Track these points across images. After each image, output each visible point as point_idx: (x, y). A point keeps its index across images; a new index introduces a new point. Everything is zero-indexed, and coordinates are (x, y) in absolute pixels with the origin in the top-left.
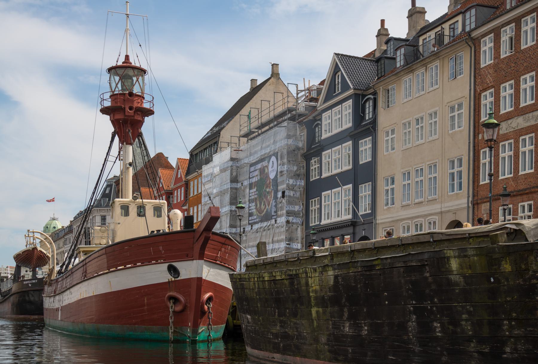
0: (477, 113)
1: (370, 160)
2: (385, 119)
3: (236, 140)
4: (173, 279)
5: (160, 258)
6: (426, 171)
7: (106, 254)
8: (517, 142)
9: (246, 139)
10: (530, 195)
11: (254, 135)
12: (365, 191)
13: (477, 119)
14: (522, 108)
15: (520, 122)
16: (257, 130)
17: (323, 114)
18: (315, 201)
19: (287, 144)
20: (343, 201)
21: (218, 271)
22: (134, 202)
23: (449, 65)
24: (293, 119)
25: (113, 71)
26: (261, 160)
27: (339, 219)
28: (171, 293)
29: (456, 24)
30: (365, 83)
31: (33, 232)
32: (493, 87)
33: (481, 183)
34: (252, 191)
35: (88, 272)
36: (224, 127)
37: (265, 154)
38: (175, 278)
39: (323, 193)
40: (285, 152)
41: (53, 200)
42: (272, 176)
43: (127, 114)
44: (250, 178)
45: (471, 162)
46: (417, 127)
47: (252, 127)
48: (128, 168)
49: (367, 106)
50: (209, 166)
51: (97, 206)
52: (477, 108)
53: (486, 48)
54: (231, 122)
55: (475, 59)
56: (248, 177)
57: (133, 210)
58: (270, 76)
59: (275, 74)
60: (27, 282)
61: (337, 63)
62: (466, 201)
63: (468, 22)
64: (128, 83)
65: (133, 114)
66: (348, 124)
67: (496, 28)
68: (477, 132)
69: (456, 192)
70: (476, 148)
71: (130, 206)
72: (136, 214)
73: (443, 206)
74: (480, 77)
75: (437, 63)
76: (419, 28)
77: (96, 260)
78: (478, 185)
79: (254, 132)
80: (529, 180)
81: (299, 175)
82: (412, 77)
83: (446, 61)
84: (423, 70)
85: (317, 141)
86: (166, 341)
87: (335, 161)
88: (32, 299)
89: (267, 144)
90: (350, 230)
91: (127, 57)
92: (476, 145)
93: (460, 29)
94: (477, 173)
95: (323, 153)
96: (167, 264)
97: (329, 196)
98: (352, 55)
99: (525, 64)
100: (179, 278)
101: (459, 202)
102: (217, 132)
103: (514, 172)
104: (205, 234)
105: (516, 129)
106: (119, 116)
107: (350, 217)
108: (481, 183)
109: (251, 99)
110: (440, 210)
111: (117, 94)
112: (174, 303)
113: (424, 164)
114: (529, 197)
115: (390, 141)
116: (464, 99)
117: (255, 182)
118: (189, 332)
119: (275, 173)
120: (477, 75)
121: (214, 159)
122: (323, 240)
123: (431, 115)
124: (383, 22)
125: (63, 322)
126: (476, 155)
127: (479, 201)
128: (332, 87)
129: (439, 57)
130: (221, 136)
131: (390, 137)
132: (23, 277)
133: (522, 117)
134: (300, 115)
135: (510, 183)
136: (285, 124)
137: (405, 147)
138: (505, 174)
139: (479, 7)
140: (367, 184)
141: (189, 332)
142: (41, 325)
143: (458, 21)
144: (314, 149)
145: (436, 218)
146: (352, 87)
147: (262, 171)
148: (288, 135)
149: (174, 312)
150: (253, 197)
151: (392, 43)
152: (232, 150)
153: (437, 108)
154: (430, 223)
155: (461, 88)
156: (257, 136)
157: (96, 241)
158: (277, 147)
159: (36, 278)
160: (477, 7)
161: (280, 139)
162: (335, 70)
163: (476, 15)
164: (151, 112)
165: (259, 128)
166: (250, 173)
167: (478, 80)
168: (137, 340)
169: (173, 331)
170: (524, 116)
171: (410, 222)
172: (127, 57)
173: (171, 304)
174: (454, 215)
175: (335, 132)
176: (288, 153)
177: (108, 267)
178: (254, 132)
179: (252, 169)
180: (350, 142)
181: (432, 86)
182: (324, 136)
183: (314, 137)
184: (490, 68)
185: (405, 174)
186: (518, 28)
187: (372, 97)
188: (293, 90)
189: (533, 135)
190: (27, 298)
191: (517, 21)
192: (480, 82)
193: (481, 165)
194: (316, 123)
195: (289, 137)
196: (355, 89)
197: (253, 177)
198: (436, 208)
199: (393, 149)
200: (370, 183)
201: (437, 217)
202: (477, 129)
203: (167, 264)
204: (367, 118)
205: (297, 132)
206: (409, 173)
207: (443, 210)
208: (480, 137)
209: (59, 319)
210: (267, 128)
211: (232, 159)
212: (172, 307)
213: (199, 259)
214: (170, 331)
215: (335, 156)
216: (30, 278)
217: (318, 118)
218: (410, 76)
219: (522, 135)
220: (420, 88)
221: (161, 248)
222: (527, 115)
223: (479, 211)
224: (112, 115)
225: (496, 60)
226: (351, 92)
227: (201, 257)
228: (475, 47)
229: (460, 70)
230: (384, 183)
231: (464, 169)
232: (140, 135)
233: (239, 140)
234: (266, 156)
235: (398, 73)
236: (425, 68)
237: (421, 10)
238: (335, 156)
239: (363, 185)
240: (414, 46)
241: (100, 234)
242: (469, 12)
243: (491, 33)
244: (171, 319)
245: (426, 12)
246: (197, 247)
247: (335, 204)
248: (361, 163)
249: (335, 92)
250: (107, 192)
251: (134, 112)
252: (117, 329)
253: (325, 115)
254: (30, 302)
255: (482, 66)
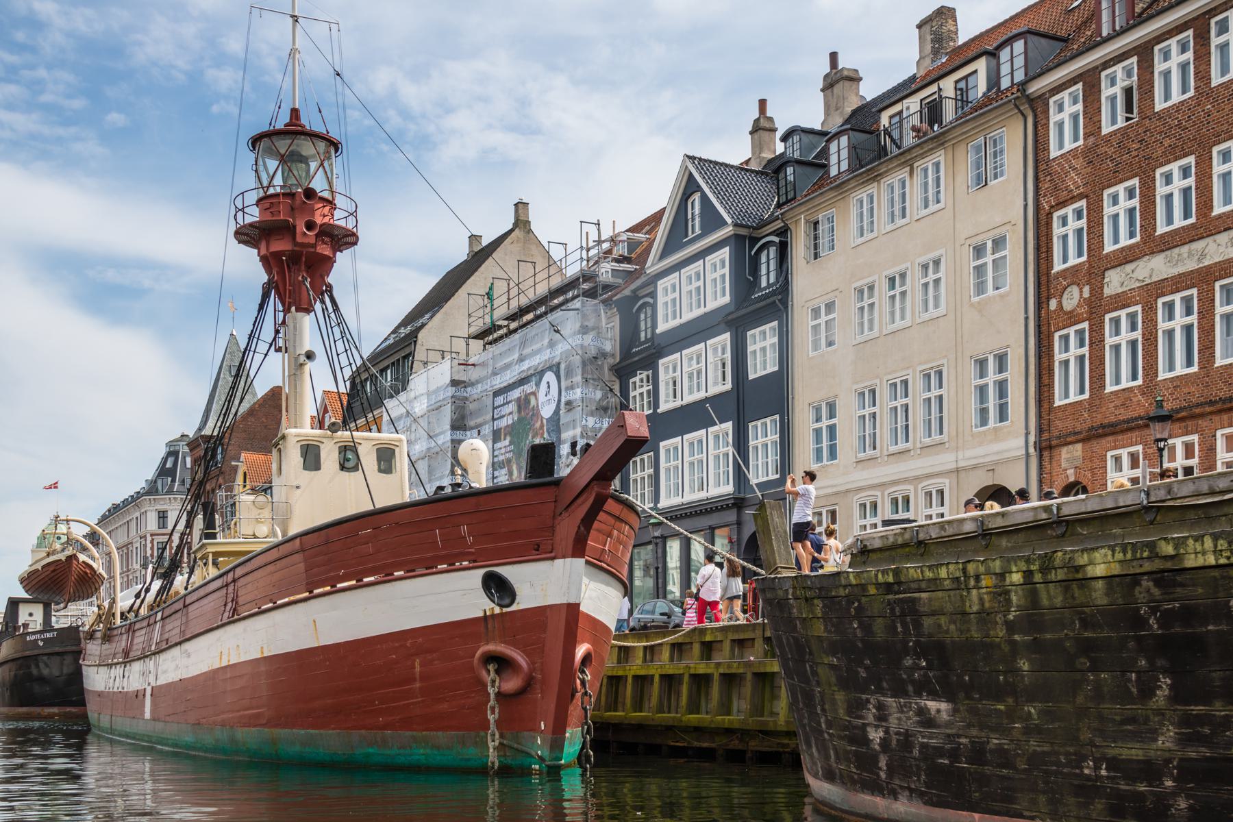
0: (1044, 255)
1: (776, 368)
2: (808, 282)
3: (460, 345)
4: (497, 610)
5: (461, 556)
6: (916, 385)
7: (302, 550)
8: (1150, 310)
9: (481, 342)
10: (1190, 423)
11: (501, 332)
12: (764, 434)
13: (1043, 267)
14: (1162, 236)
15: (1157, 267)
16: (506, 323)
17: (659, 283)
18: (642, 460)
19: (582, 345)
20: (686, 466)
21: (603, 587)
22: (332, 437)
23: (966, 159)
24: (591, 294)
25: (264, 143)
26: (522, 381)
27: (702, 495)
28: (491, 647)
29: (970, 79)
30: (763, 211)
31: (67, 521)
32: (1081, 196)
33: (1057, 403)
34: (498, 445)
35: (241, 600)
36: (423, 325)
37: (529, 369)
38: (501, 606)
39: (662, 444)
40: (577, 360)
41: (55, 486)
42: (547, 412)
43: (299, 239)
44: (494, 419)
45: (1032, 360)
46: (892, 293)
47: (497, 314)
48: (301, 365)
49: (764, 259)
50: (403, 397)
51: (149, 493)
52: (1043, 244)
53: (1065, 116)
54: (439, 316)
55: (1036, 141)
56: (489, 417)
57: (329, 456)
58: (511, 227)
59: (521, 222)
60: (33, 638)
61: (691, 174)
62: (1021, 442)
63: (1005, 69)
64: (298, 170)
65: (313, 241)
66: (719, 298)
67: (1088, 71)
68: (1044, 294)
69: (825, 462)
70: (1044, 328)
71: (322, 446)
72: (338, 466)
73: (960, 457)
74: (1048, 178)
75: (940, 156)
76: (848, 110)
77: (270, 568)
78: (1051, 409)
79: (500, 327)
80: (1186, 390)
81: (605, 409)
82: (875, 190)
83: (960, 151)
84: (904, 173)
85: (643, 339)
86: (483, 771)
87: (690, 377)
88: (45, 672)
89: (536, 347)
90: (731, 516)
91: (295, 113)
92: (1044, 322)
93: (982, 87)
94: (1046, 382)
95: (661, 362)
96: (482, 572)
97: (700, 442)
98: (720, 161)
99: (1167, 142)
100: (514, 608)
101: (1006, 450)
102: (407, 336)
103: (1145, 375)
104: (596, 489)
105: (1148, 281)
106: (280, 245)
107: (729, 489)
108: (1057, 403)
109: (476, 270)
110: (954, 466)
111: (276, 195)
112: (497, 672)
113: (910, 371)
114: (1186, 427)
115: (823, 327)
116: (1008, 227)
117: (508, 426)
118: (539, 746)
119: (553, 406)
120: (1041, 175)
121: (412, 385)
122: (712, 529)
123: (861, 292)
124: (763, 103)
125: (159, 726)
126: (1045, 343)
127: (1054, 442)
128: (679, 226)
129: (942, 144)
130: (419, 342)
131: (824, 318)
132: (25, 626)
133: (1163, 255)
134: (606, 287)
135: (1134, 400)
136: (577, 304)
137: (860, 339)
138: (1121, 378)
139: (1036, 38)
140: (768, 420)
141: (539, 746)
142: (78, 735)
143: (976, 71)
144: (637, 357)
145: (945, 483)
146: (729, 221)
147: (523, 403)
148: (582, 327)
149: (499, 695)
150: (501, 458)
151: (796, 138)
152: (456, 362)
153: (942, 251)
154: (929, 494)
155: (1006, 202)
156: (501, 337)
157: (246, 529)
158: (558, 353)
159: (52, 630)
160: (1031, 38)
161: (578, 333)
162: (689, 187)
163: (1026, 52)
164: (350, 239)
165: (512, 318)
166: (494, 408)
167: (1045, 186)
168: (392, 769)
169: (497, 743)
170: (1168, 253)
171: (879, 493)
172: (295, 113)
173: (489, 675)
174: (991, 473)
175: (687, 316)
176: (584, 364)
177: (307, 584)
178: (500, 327)
179: (500, 400)
180: (727, 336)
181: (862, 235)
182: (662, 327)
183: (637, 331)
184: (1075, 157)
185: (863, 394)
186: (1146, 66)
187: (776, 239)
188: (556, 253)
189: (1194, 291)
190: (35, 671)
191: (1144, 52)
192: (1048, 187)
193: (1057, 364)
194: (640, 302)
195: (584, 330)
196: (736, 225)
197: (503, 417)
198: (945, 460)
199: (830, 344)
200: (777, 417)
201: (947, 481)
202: (1043, 288)
203: (482, 572)
204: (764, 284)
205: (600, 320)
206: (873, 392)
207: (962, 464)
208: (1053, 304)
209: (147, 715)
210: (530, 316)
211: (454, 383)
212: (493, 681)
213: (573, 556)
214: (491, 745)
215: (690, 365)
216: (39, 628)
217: (649, 290)
218: (872, 188)
219: (1163, 295)
220: (896, 213)
221: (464, 530)
222: (1176, 250)
223: (1054, 464)
224: (263, 246)
225: (1091, 140)
226: (727, 231)
227: (578, 550)
228: (1035, 116)
229: (996, 168)
230: (812, 416)
231: (1015, 375)
232: (330, 288)
233: (468, 345)
234: (532, 371)
235: (843, 183)
236: (908, 169)
237: (851, 74)
238: (690, 365)
239: (759, 423)
240: (871, 133)
241: (255, 513)
242: (1009, 48)
243: (1076, 83)
244: (493, 712)
245: (861, 79)
246: (567, 527)
247: (692, 464)
248: (751, 376)
249: (687, 236)
250: (169, 465)
251: (317, 235)
252: (329, 741)
253: (661, 284)
254: (42, 679)
255: (1054, 153)
